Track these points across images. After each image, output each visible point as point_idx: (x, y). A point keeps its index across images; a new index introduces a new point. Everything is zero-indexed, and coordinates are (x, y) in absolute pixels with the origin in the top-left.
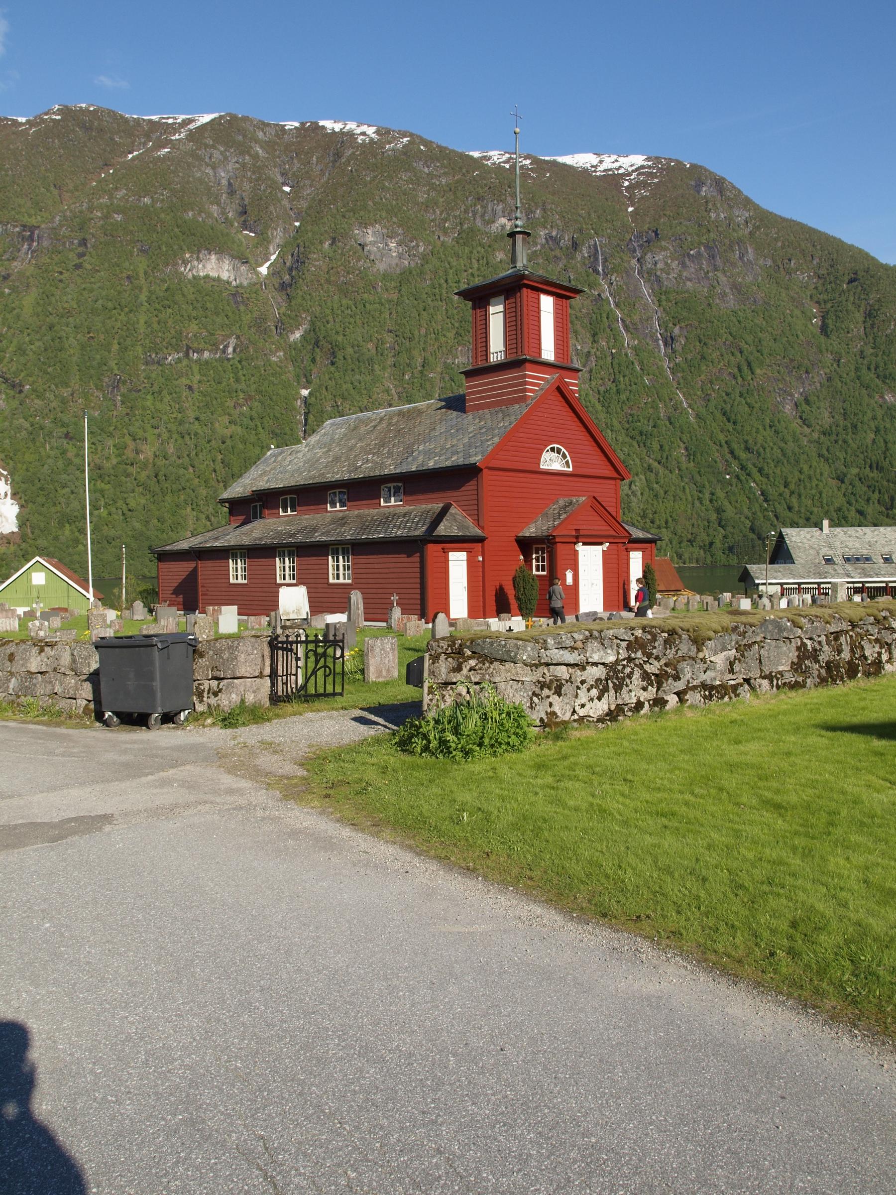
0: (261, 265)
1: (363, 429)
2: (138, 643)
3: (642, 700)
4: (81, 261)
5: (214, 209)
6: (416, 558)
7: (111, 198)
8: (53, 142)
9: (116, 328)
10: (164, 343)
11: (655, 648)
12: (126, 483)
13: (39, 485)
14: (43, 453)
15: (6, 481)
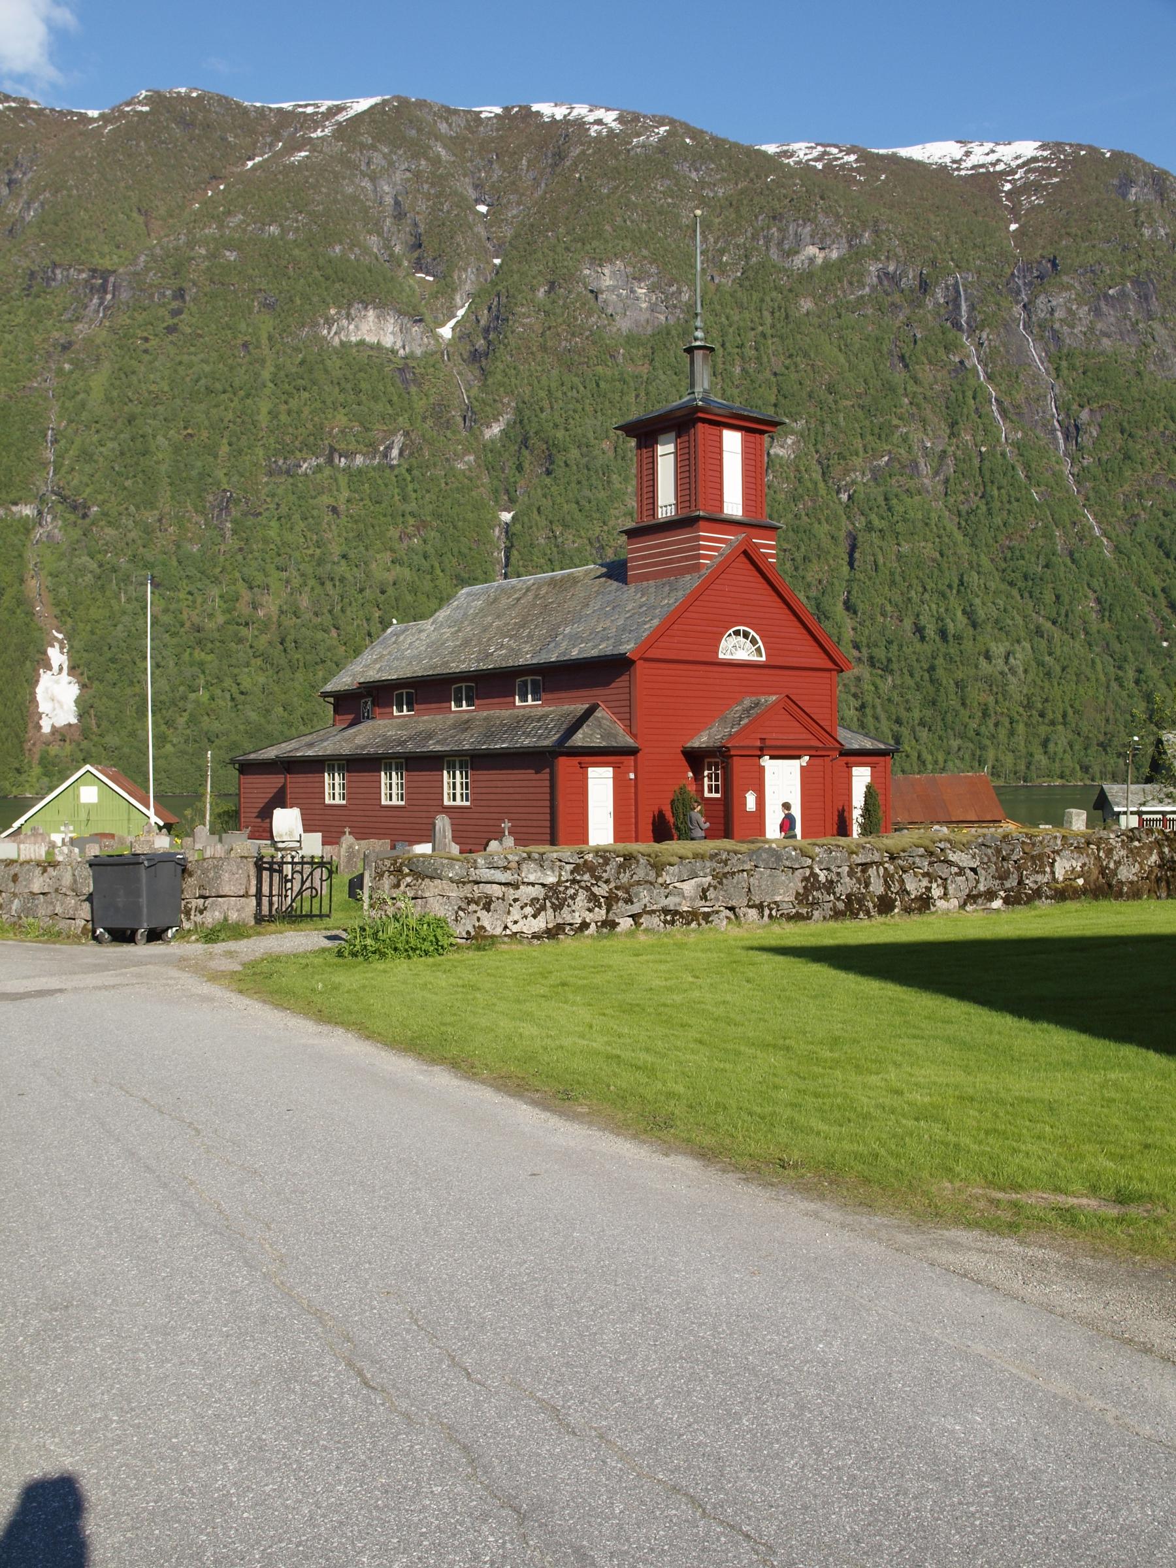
0: (442, 325)
1: (504, 602)
2: (127, 861)
3: (588, 920)
4: (175, 321)
5: (373, 241)
6: (545, 774)
7: (221, 227)
8: (138, 145)
9: (226, 420)
10: (297, 443)
11: (605, 871)
12: (238, 651)
13: (109, 655)
14: (116, 608)
15: (61, 648)
